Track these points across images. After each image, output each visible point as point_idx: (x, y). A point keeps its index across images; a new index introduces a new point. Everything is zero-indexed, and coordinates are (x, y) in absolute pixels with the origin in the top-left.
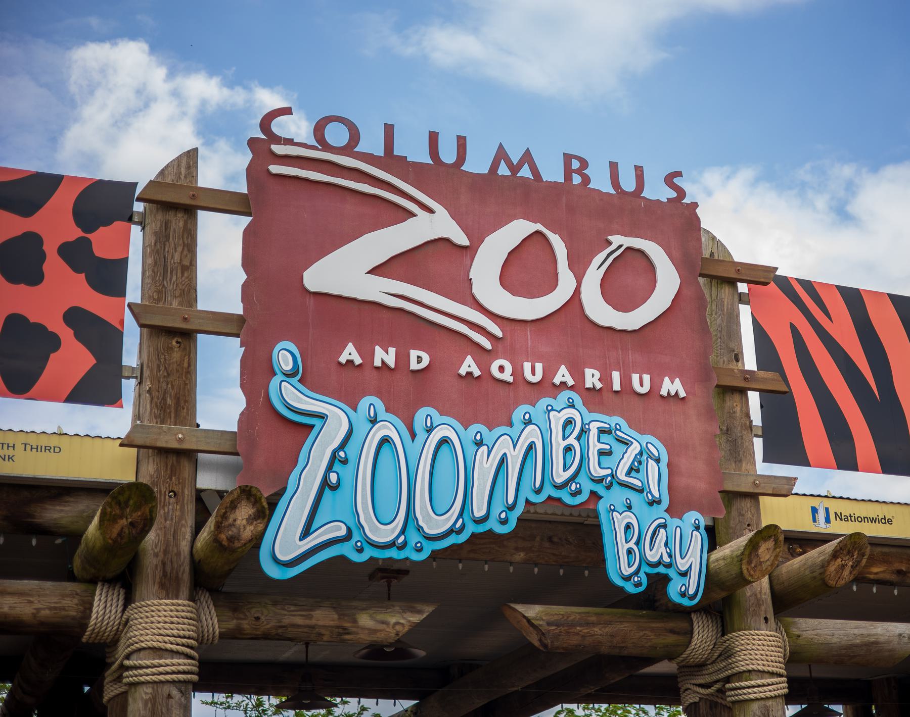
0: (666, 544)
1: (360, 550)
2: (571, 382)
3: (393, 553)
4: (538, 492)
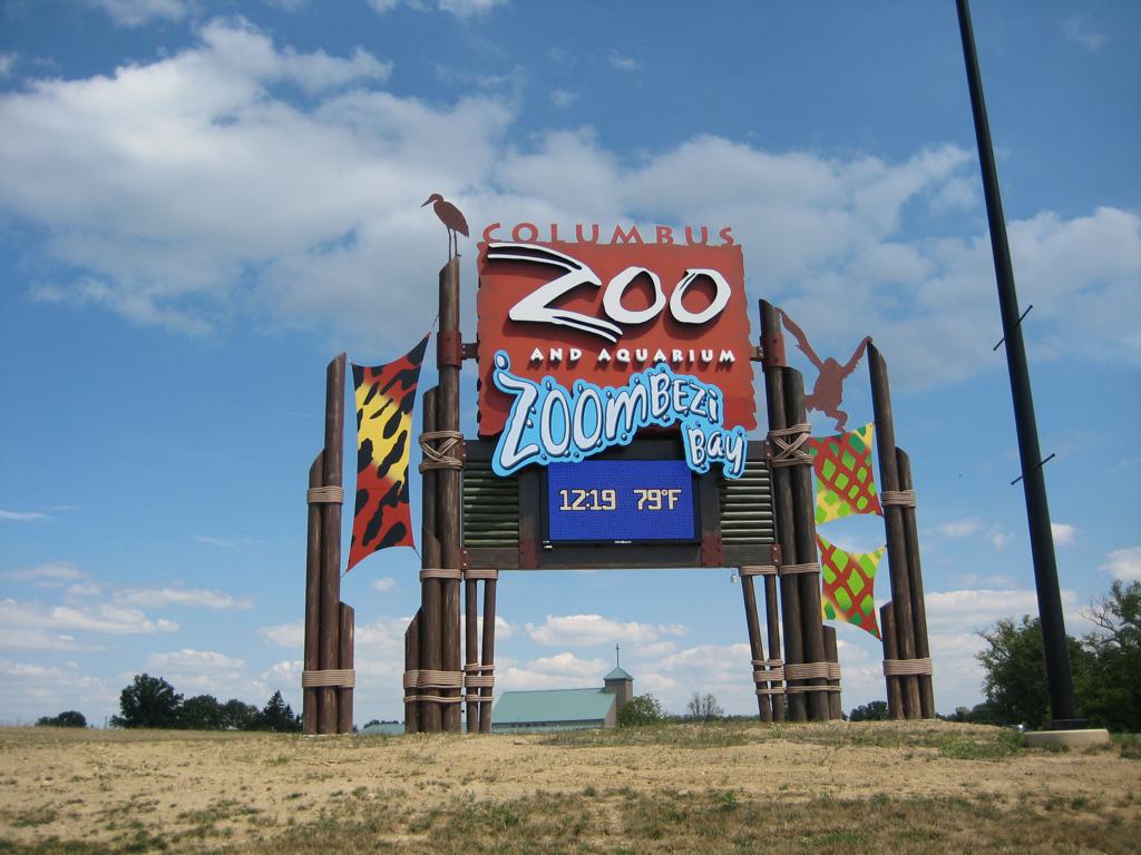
0: (721, 445)
1: (545, 459)
2: (664, 358)
3: (563, 459)
4: (644, 421)
